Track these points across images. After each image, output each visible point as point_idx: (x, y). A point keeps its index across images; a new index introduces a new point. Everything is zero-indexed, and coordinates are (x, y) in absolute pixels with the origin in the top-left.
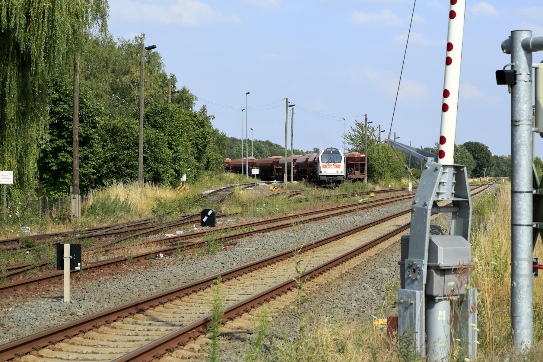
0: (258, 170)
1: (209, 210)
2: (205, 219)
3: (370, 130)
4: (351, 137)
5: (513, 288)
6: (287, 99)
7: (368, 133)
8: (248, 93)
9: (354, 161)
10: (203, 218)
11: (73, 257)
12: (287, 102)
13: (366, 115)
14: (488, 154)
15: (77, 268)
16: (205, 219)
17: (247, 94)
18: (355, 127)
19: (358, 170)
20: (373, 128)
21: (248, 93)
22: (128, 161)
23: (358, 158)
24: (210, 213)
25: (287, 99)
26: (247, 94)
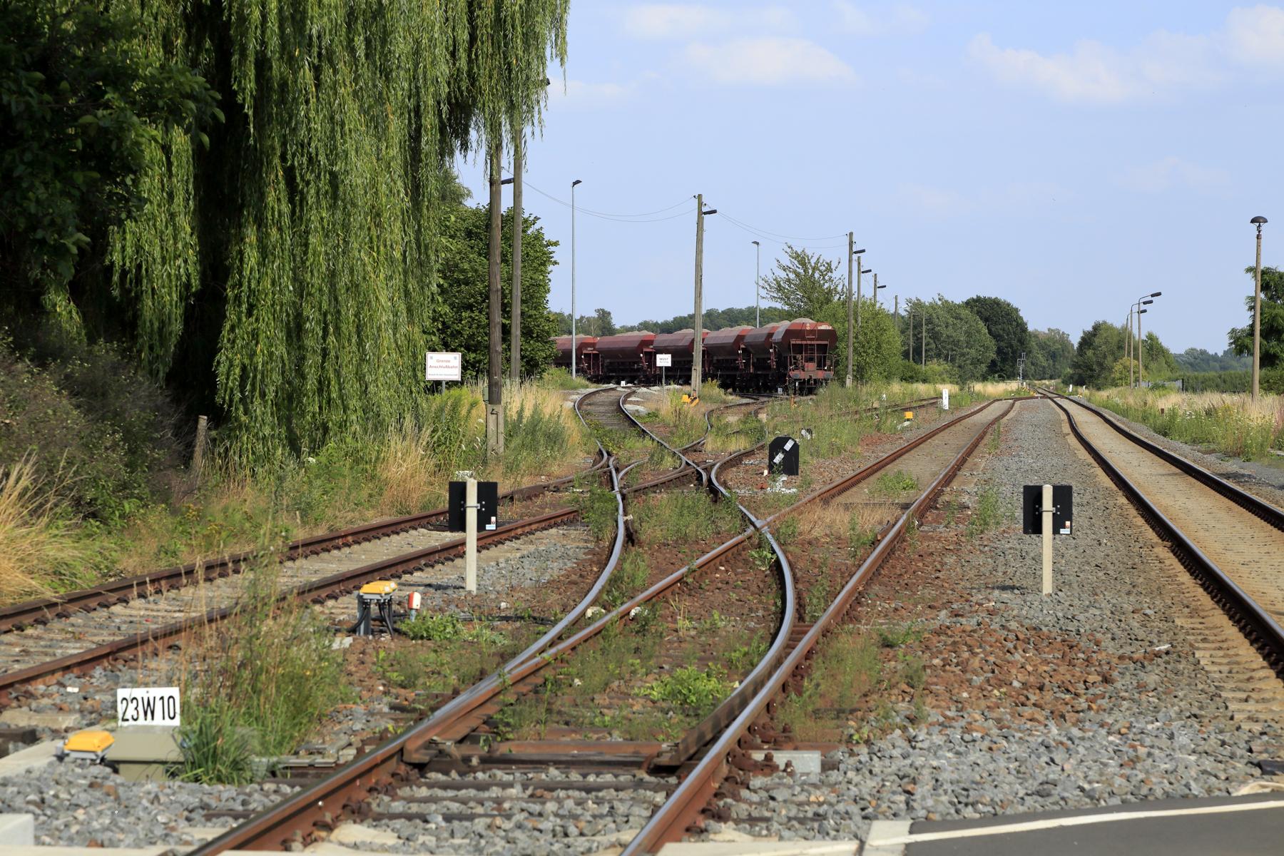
0: (669, 357)
1: (786, 440)
2: (778, 458)
3: (823, 268)
4: (779, 288)
5: (585, 641)
6: (700, 196)
7: (817, 275)
8: (578, 182)
9: (804, 339)
10: (772, 457)
11: (482, 506)
12: (700, 204)
13: (851, 234)
14: (1022, 327)
15: (488, 527)
16: (778, 458)
17: (575, 183)
18: (786, 261)
19: (811, 360)
20: (829, 264)
21: (578, 182)
22: (472, 337)
23: (812, 332)
24: (788, 446)
25: (700, 196)
26: (575, 183)
